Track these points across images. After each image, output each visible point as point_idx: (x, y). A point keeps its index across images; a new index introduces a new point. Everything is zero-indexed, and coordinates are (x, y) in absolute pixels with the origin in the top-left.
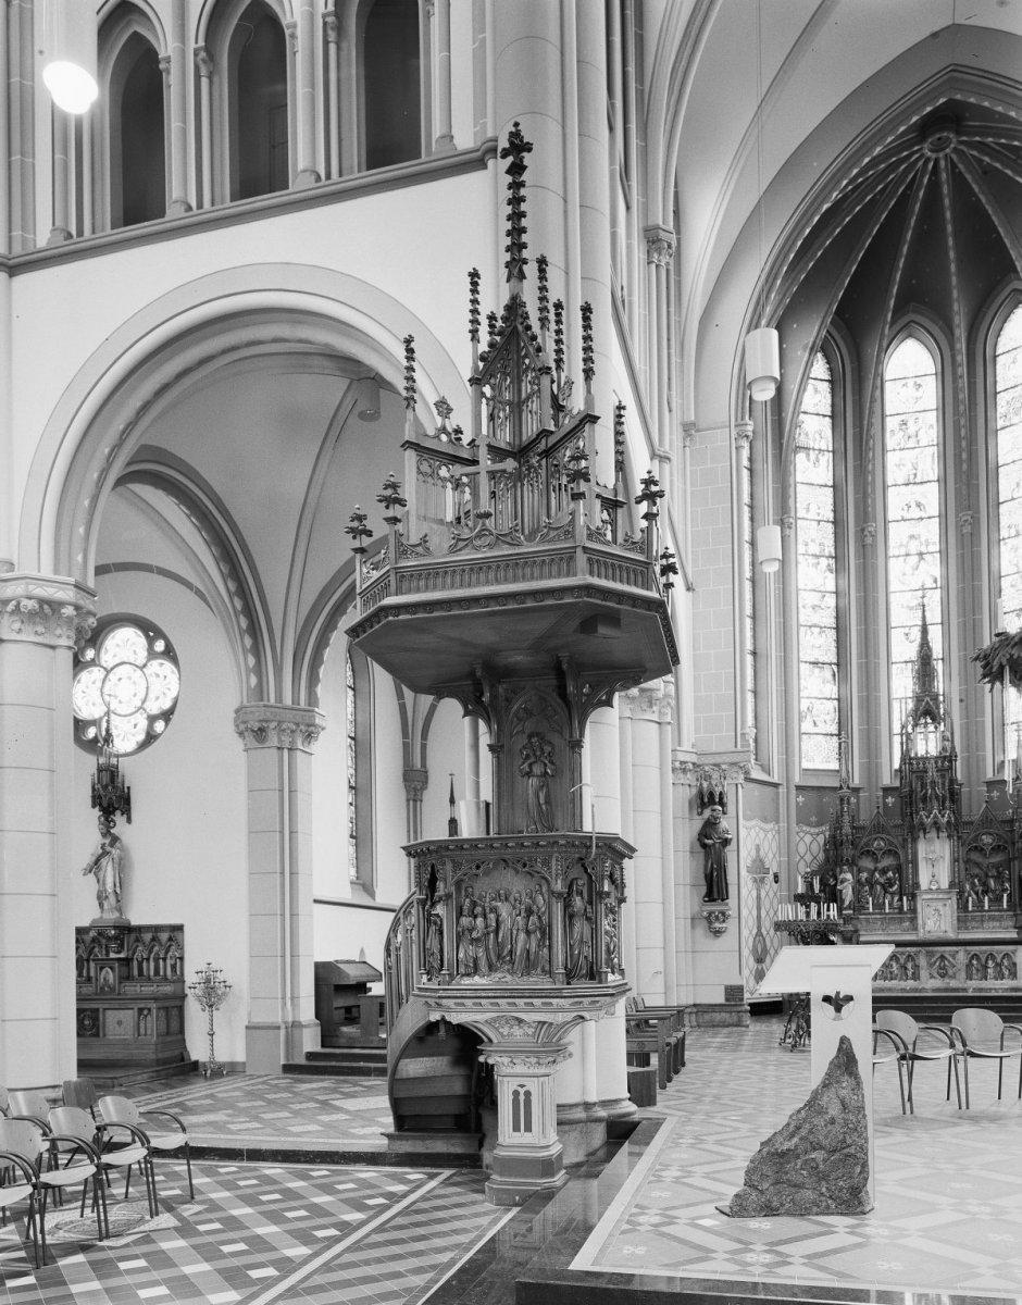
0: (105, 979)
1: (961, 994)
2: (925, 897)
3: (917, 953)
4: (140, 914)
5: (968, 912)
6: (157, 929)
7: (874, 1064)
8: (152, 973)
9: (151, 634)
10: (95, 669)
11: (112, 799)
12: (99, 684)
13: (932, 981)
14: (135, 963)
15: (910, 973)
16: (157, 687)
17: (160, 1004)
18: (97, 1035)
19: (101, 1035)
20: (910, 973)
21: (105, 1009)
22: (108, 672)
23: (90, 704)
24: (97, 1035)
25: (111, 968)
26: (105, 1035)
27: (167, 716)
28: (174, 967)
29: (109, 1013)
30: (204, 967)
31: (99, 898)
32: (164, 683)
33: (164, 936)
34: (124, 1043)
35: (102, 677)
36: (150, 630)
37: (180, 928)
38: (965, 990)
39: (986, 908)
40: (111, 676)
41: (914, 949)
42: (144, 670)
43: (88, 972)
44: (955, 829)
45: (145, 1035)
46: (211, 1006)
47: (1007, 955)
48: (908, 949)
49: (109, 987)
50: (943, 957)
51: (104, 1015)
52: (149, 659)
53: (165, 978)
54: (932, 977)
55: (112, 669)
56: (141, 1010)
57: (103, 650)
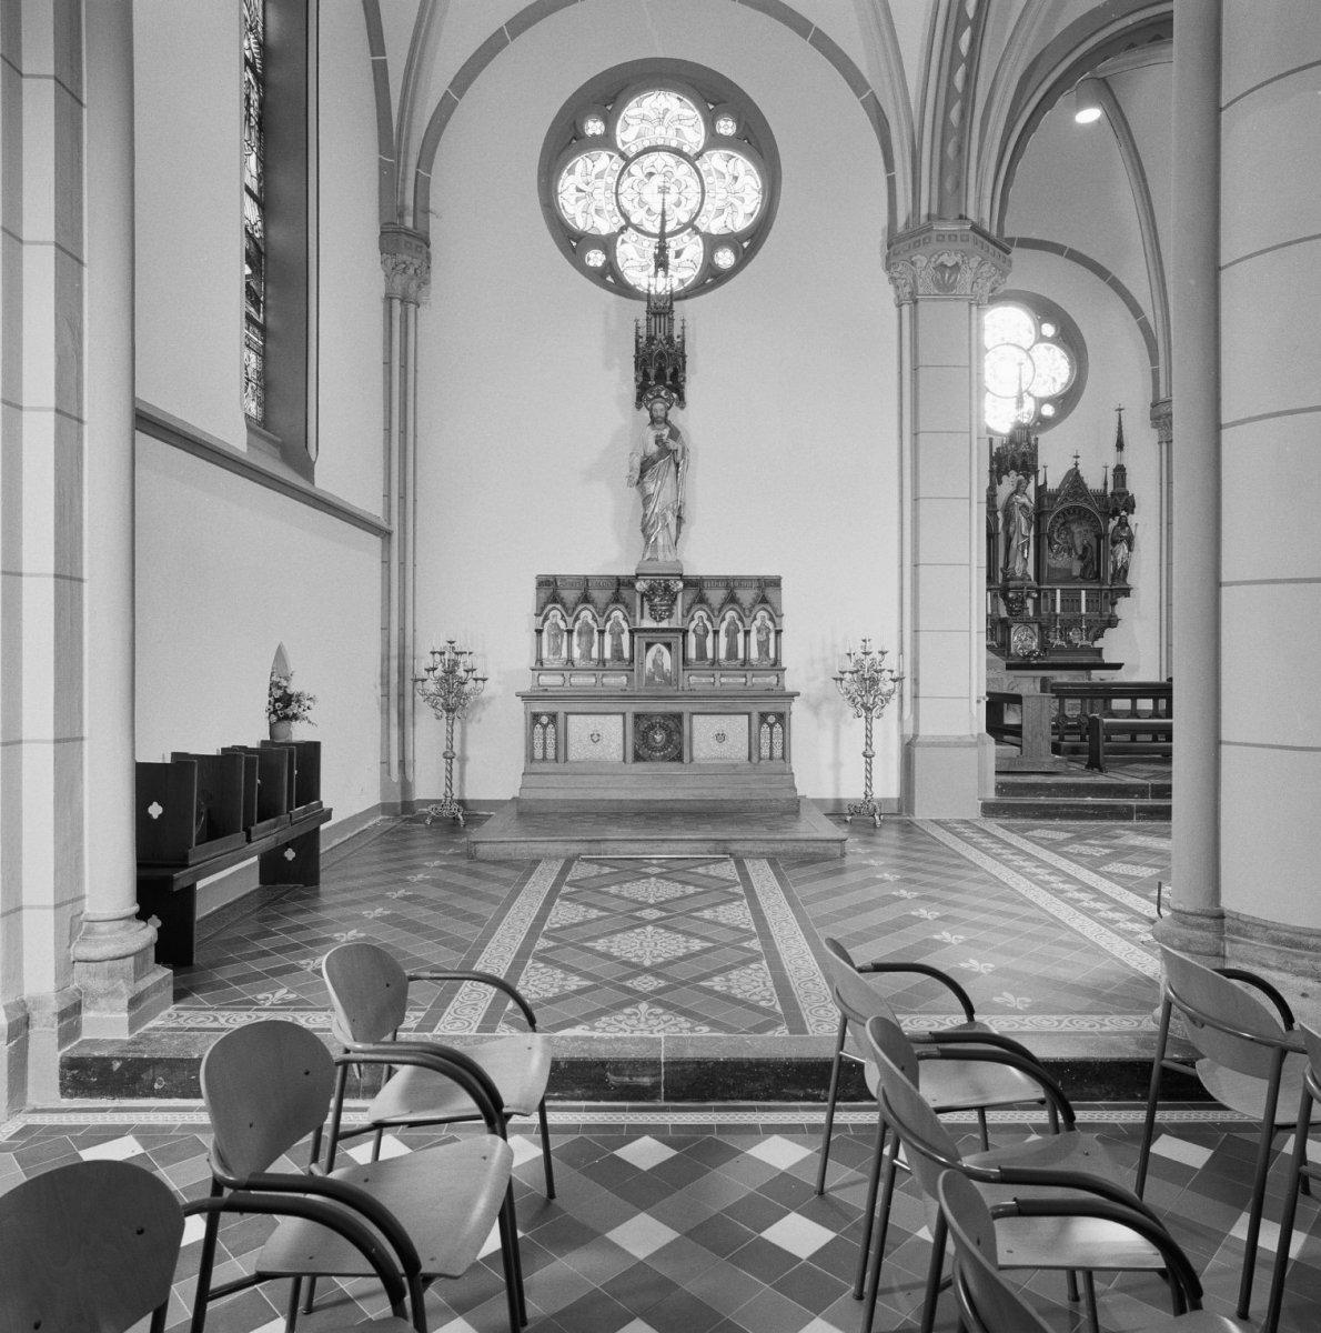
0: (654, 662)
4: (707, 552)
6: (731, 585)
7: (624, 714)
8: (722, 654)
9: (746, 244)
10: (1032, 337)
11: (660, 370)
12: (612, 180)
14: (692, 639)
16: (718, 193)
18: (679, 758)
19: (686, 758)
21: (567, 714)
22: (628, 160)
23: (592, 211)
24: (679, 758)
25: (668, 646)
26: (692, 760)
28: (763, 646)
29: (571, 718)
30: (441, 645)
31: (643, 531)
32: (734, 192)
33: (746, 596)
34: (732, 770)
36: (711, 92)
37: (775, 583)
39: (1083, 592)
40: (634, 168)
42: (623, 223)
43: (601, 651)
45: (771, 758)
46: (868, 710)
49: (663, 676)
52: (1036, 342)
53: (715, 661)
55: (639, 155)
56: (763, 716)
57: (620, 124)
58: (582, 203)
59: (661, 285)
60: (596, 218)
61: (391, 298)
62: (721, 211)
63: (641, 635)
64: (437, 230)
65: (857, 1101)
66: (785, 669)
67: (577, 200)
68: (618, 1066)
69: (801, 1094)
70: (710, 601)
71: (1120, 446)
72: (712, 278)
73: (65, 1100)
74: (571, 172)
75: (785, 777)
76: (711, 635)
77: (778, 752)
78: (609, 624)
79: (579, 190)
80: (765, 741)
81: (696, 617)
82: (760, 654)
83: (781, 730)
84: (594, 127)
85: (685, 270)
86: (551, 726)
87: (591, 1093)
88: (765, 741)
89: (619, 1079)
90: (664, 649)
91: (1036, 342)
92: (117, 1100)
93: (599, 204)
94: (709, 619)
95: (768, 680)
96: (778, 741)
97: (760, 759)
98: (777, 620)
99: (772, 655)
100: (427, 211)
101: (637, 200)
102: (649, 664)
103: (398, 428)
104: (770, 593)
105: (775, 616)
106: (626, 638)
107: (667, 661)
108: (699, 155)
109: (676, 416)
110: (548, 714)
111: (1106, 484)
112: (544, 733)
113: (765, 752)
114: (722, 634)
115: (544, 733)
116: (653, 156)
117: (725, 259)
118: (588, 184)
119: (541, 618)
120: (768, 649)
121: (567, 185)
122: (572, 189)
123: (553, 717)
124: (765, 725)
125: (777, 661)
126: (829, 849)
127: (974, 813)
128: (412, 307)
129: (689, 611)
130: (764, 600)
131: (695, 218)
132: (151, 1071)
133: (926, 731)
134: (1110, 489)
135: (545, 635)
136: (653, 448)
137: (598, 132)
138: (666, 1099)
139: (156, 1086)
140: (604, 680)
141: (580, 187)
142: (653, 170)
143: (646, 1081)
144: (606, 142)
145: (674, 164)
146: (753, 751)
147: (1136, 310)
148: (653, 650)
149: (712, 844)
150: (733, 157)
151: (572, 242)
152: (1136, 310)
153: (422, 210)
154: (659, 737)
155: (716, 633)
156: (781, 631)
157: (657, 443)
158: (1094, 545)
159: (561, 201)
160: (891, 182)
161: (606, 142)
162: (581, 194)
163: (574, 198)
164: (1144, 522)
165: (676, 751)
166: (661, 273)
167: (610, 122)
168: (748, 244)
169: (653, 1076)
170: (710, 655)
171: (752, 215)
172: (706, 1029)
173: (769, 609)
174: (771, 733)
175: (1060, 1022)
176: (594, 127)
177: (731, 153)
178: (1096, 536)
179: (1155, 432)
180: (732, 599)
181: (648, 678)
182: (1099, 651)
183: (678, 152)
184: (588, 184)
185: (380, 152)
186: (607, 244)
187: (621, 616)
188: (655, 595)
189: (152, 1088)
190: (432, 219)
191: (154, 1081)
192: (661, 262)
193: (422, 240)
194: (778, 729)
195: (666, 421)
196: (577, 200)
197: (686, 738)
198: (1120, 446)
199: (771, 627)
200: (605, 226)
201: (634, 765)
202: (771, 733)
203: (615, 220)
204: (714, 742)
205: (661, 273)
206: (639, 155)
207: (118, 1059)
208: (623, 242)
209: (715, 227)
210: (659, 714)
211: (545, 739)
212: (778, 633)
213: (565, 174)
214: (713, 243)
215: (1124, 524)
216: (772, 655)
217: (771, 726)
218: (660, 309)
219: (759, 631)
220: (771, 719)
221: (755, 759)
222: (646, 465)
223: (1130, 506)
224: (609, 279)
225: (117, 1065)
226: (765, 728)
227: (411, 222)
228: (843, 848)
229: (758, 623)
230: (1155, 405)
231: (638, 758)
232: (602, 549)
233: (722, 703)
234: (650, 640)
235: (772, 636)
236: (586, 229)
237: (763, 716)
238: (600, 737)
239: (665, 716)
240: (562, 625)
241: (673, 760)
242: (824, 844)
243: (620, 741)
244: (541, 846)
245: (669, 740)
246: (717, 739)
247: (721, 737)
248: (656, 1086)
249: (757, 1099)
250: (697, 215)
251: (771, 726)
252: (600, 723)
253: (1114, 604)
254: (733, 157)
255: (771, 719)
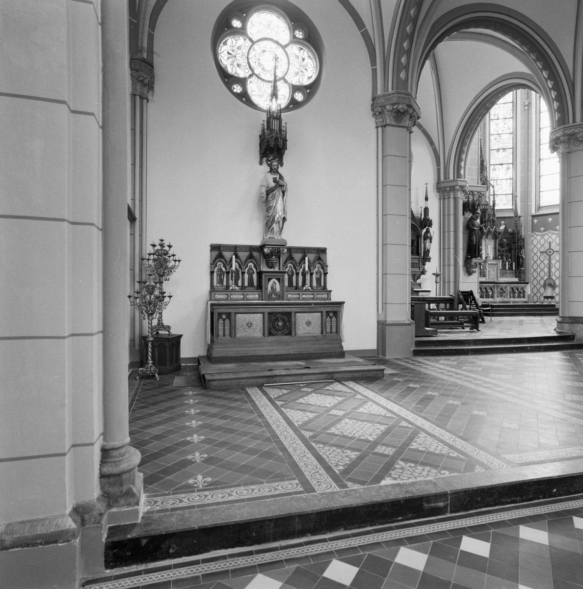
0: (272, 288)
1: (508, 304)
2: (489, 263)
3: (494, 286)
4: (295, 236)
5: (506, 270)
6: (305, 251)
8: (300, 284)
11: (273, 147)
13: (498, 298)
15: (522, 295)
17: (324, 310)
18: (290, 334)
19: (293, 334)
20: (522, 295)
21: (236, 313)
24: (290, 334)
25: (278, 280)
26: (295, 335)
27: (244, 97)
28: (319, 280)
29: (298, 315)
32: (302, 67)
34: (315, 339)
35: (281, 42)
37: (323, 251)
38: (509, 302)
40: (256, 46)
41: (493, 285)
44: (495, 237)
45: (331, 332)
47: (522, 288)
48: (491, 284)
49: (276, 294)
50: (501, 289)
51: (295, 316)
52: (291, 42)
53: (297, 288)
54: (498, 297)
55: (258, 41)
58: (231, 60)
59: (274, 107)
60: (238, 68)
61: (135, 95)
62: (297, 74)
63: (266, 274)
64: (157, 61)
65: (532, 501)
66: (331, 291)
67: (228, 58)
68: (428, 498)
69: (509, 500)
70: (295, 259)
71: (427, 199)
72: (294, 104)
73: (108, 571)
74: (225, 44)
75: (338, 341)
76: (295, 275)
77: (334, 330)
78: (247, 269)
79: (229, 53)
80: (328, 325)
81: (288, 266)
82: (317, 284)
83: (229, 322)
84: (236, 23)
85: (283, 99)
86: (334, 317)
87: (415, 515)
88: (328, 325)
89: (429, 505)
90: (276, 281)
91: (291, 42)
92: (144, 565)
93: (239, 62)
94: (295, 268)
95: (323, 296)
96: (334, 325)
97: (326, 333)
98: (325, 268)
99: (322, 285)
100: (152, 52)
101: (257, 62)
102: (269, 289)
103: (139, 165)
104: (322, 256)
105: (324, 266)
106: (255, 276)
107: (278, 287)
108: (287, 46)
109: (280, 170)
110: (332, 312)
111: (421, 214)
112: (224, 323)
113: (328, 330)
114: (300, 274)
115: (224, 323)
116: (265, 42)
117: (299, 97)
118: (233, 51)
119: (214, 266)
120: (321, 281)
121: (223, 51)
122: (226, 53)
123: (229, 315)
124: (221, 320)
125: (325, 288)
126: (377, 374)
127: (410, 355)
128: (145, 101)
129: (285, 263)
130: (319, 259)
131: (285, 75)
132: (168, 541)
133: (390, 319)
134: (423, 217)
135: (215, 274)
136: (273, 184)
137: (235, 87)
138: (451, 512)
139: (171, 551)
140: (248, 296)
141: (229, 51)
142: (265, 49)
143: (441, 504)
144: (242, 32)
145: (255, 52)
146: (324, 330)
147: (431, 143)
148: (271, 282)
149: (326, 375)
150: (302, 49)
151: (228, 79)
152: (431, 143)
153: (151, 51)
154: (280, 323)
155: (297, 274)
156: (327, 273)
157: (274, 181)
158: (416, 239)
159: (220, 57)
160: (374, 71)
161: (242, 32)
162: (229, 56)
163: (227, 57)
164: (434, 230)
165: (288, 329)
166: (274, 100)
167: (244, 22)
168: (310, 90)
169: (444, 501)
170: (294, 284)
171: (311, 77)
172: (447, 472)
173: (321, 262)
174: (331, 321)
175: (253, 490)
176: (236, 23)
177: (302, 47)
178: (417, 236)
179: (438, 194)
180: (291, 258)
181: (269, 295)
182: (420, 285)
183: (277, 43)
184: (233, 51)
185: (130, 16)
186: (242, 82)
187: (253, 266)
188: (269, 257)
189: (168, 552)
190: (155, 56)
191: (169, 548)
192: (274, 95)
193: (149, 65)
194: (334, 319)
195: (278, 172)
196: (228, 58)
197: (293, 326)
198: (427, 199)
199: (322, 272)
200: (242, 73)
201: (268, 338)
202: (331, 321)
203: (247, 71)
204: (305, 326)
205: (274, 100)
206: (258, 41)
207: (145, 537)
208: (251, 82)
209: (295, 81)
210: (280, 313)
211: (224, 326)
212: (325, 274)
213: (222, 44)
214: (295, 89)
215: (428, 231)
216: (322, 285)
217: (331, 318)
218: (273, 118)
219: (317, 273)
220: (224, 316)
221: (324, 333)
222: (269, 191)
223: (430, 224)
224: (244, 99)
225: (144, 541)
226: (328, 319)
227: (146, 56)
228: (383, 373)
229: (316, 269)
230: (438, 183)
231: (270, 334)
232: (250, 235)
233: (308, 307)
234: (269, 277)
235: (322, 276)
236: (233, 73)
237: (328, 313)
238: (251, 325)
239: (282, 313)
240: (224, 269)
241: (287, 335)
242: (376, 372)
243: (261, 326)
244: (244, 381)
245: (284, 325)
246: (307, 324)
247: (309, 323)
248: (446, 507)
249: (490, 506)
250: (286, 74)
251: (331, 318)
252: (251, 317)
253: (424, 264)
254: (302, 49)
255: (224, 316)
